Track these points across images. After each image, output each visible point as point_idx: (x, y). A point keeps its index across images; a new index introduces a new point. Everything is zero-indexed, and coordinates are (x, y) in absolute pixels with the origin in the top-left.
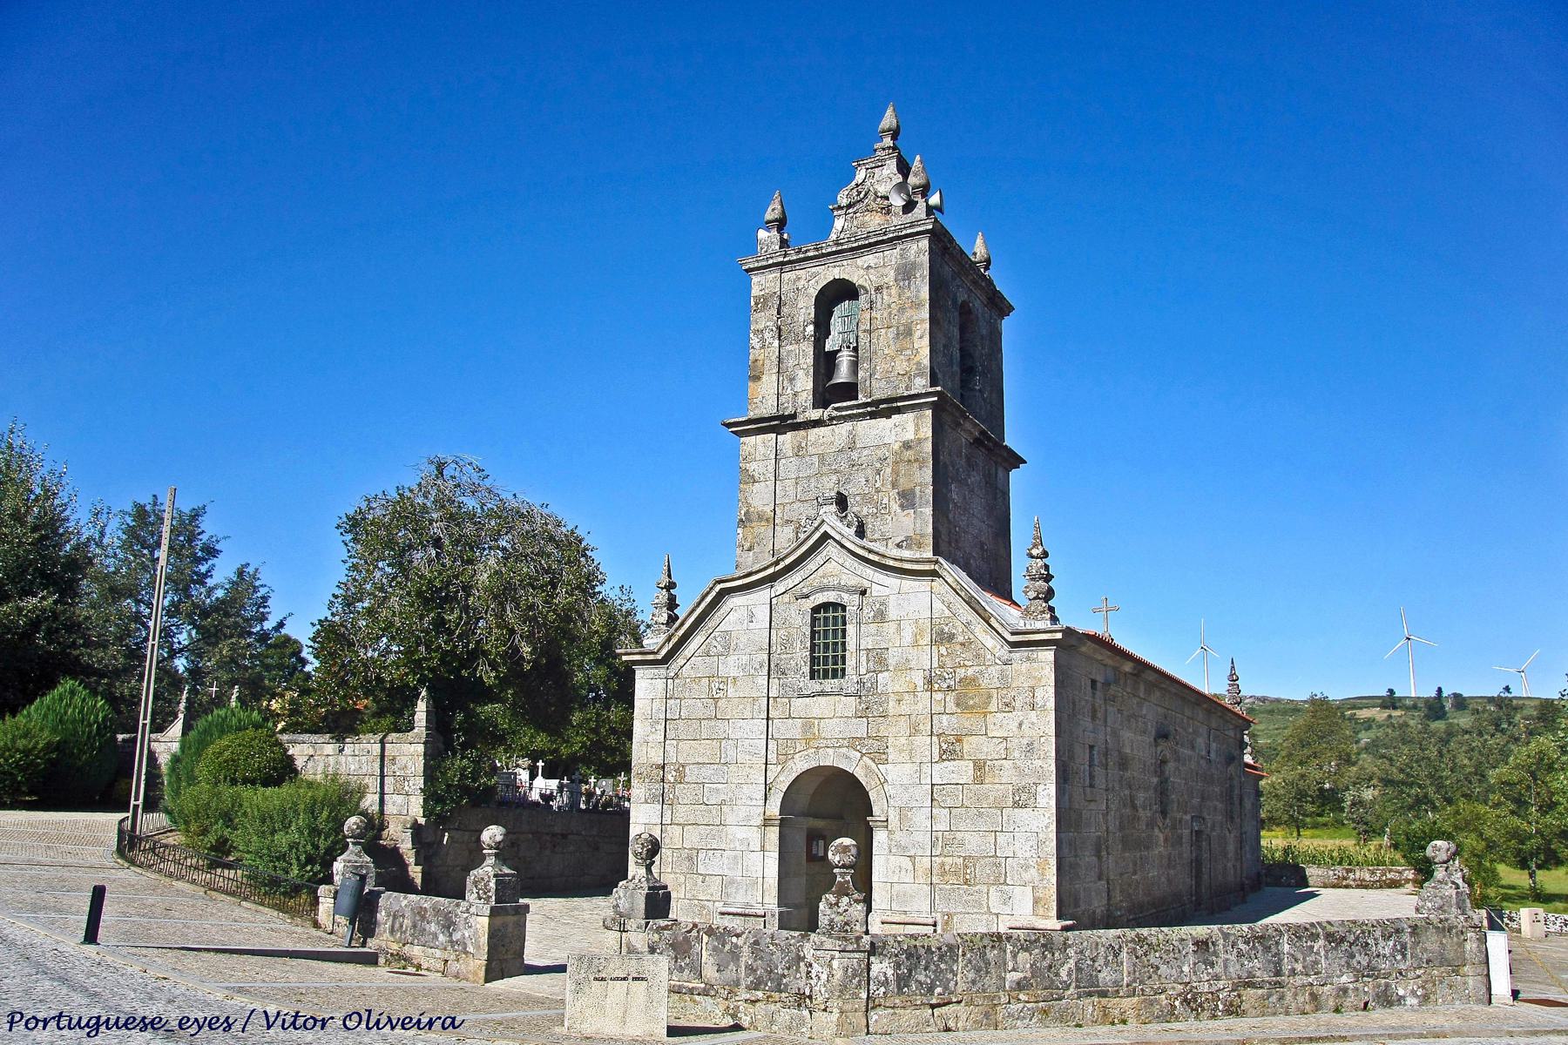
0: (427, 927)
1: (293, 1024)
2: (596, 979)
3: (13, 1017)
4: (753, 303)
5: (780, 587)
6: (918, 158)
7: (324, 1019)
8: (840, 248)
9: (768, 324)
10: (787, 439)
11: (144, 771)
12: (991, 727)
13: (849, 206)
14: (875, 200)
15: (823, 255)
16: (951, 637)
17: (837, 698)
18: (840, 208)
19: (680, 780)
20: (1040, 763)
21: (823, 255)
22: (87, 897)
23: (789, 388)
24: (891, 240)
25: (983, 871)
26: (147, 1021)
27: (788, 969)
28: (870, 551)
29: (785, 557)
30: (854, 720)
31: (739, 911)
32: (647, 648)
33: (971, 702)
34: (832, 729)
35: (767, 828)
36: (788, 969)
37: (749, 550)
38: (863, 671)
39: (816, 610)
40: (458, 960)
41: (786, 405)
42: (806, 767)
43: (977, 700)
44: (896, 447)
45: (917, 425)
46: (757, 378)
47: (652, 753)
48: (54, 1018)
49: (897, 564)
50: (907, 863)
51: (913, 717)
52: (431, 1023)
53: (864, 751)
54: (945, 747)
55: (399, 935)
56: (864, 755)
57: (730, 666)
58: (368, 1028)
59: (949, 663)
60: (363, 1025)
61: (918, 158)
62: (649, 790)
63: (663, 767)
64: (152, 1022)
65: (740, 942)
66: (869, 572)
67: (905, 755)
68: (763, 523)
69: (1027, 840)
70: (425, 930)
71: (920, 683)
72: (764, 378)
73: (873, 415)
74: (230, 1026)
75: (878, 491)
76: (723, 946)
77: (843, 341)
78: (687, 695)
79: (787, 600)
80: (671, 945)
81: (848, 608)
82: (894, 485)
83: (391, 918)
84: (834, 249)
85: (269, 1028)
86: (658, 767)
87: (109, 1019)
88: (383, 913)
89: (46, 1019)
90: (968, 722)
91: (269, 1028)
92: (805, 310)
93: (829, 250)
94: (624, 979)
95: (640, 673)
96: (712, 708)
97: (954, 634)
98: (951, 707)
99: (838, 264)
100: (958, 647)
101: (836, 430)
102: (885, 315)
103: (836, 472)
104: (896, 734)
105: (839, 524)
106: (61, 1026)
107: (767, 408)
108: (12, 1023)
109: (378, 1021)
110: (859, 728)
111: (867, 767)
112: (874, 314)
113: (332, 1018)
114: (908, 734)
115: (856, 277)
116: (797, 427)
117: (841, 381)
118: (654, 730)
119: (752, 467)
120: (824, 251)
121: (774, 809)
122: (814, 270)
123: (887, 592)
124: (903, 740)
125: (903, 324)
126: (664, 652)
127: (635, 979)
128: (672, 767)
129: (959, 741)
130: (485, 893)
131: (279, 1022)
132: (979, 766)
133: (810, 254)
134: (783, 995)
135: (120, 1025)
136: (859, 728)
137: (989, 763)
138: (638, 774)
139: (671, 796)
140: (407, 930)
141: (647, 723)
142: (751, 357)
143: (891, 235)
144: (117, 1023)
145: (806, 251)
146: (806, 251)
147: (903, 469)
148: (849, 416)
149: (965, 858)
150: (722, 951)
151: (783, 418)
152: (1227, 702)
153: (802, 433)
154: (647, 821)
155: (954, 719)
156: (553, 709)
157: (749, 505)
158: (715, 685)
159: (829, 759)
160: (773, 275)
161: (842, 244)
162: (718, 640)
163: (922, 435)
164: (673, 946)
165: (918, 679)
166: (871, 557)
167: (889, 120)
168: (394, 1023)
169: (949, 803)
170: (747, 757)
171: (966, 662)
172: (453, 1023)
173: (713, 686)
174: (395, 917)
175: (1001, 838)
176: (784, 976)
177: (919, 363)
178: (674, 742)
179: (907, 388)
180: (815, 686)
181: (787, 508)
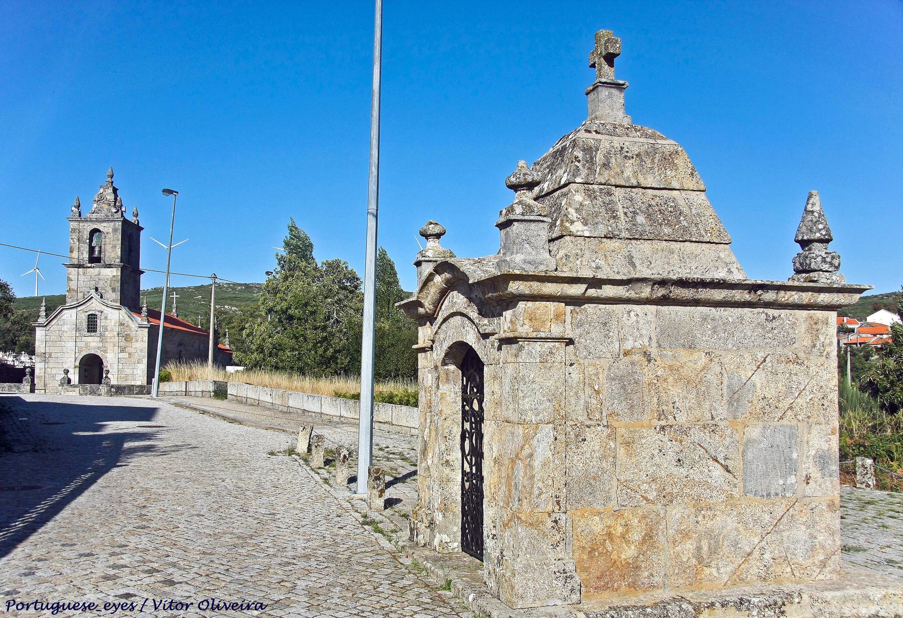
3: (9, 603)
5: (79, 309)
13: (99, 201)
26: (86, 605)
39: (89, 315)
48: (33, 603)
57: (65, 328)
64: (89, 606)
67: (112, 352)
72: (74, 252)
73: (105, 267)
92: (86, 235)
103: (95, 281)
104: (110, 347)
108: (9, 606)
121: (77, 364)
122: (89, 224)
123: (108, 312)
131: (162, 605)
132: (130, 354)
144: (69, 606)
159: (93, 352)
165: (116, 334)
169: (122, 362)
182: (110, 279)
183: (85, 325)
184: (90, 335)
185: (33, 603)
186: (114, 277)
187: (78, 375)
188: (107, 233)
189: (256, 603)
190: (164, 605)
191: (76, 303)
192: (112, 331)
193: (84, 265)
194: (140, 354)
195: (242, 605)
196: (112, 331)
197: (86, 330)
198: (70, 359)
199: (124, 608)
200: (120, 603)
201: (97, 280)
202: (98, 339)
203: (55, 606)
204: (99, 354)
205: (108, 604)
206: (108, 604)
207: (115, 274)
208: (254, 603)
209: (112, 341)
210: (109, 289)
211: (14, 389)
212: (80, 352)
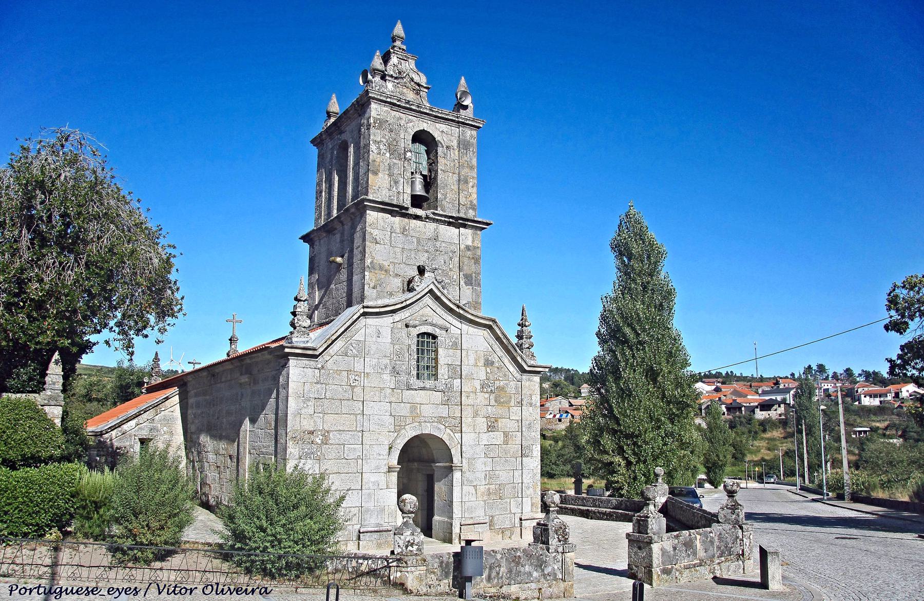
1: (174, 591)
3: (12, 588)
5: (397, 317)
7: (191, 589)
8: (431, 113)
9: (383, 139)
12: (511, 414)
16: (493, 363)
17: (431, 392)
19: (325, 442)
23: (395, 188)
24: (458, 122)
25: (508, 490)
26: (90, 590)
31: (376, 529)
32: (295, 345)
33: (502, 400)
34: (427, 411)
35: (390, 473)
42: (414, 434)
45: (473, 238)
47: (305, 423)
48: (35, 588)
49: (472, 318)
50: (472, 490)
51: (475, 407)
52: (253, 591)
53: (447, 425)
55: (496, 580)
56: (446, 427)
58: (217, 594)
60: (214, 592)
62: (302, 449)
64: (92, 591)
66: (450, 318)
71: (478, 387)
72: (380, 175)
73: (450, 224)
74: (137, 592)
75: (451, 270)
78: (331, 382)
80: (684, 544)
84: (428, 112)
85: (160, 593)
87: (67, 588)
89: (31, 589)
90: (500, 411)
91: (160, 593)
93: (425, 111)
95: (292, 362)
96: (350, 392)
98: (493, 402)
99: (425, 121)
101: (427, 225)
102: (452, 165)
106: (40, 593)
108: (11, 591)
109: (223, 589)
110: (443, 411)
113: (196, 588)
114: (472, 416)
115: (437, 136)
118: (305, 405)
122: (410, 117)
124: (470, 420)
128: (319, 433)
129: (496, 421)
131: (166, 590)
132: (506, 434)
133: (413, 107)
135: (74, 592)
136: (443, 411)
137: (510, 433)
138: (292, 437)
139: (319, 453)
143: (461, 120)
144: (72, 591)
145: (412, 105)
146: (412, 105)
148: (441, 220)
149: (500, 485)
153: (406, 220)
159: (427, 429)
161: (433, 111)
162: (354, 345)
168: (232, 591)
170: (377, 427)
172: (266, 591)
173: (350, 377)
177: (471, 202)
178: (321, 415)
181: (397, 266)
184: (422, 385)
185: (35, 588)
186: (469, 250)
188: (447, 147)
189: (260, 588)
190: (168, 589)
195: (246, 590)
199: (128, 593)
200: (123, 588)
203: (57, 591)
205: (111, 589)
206: (111, 589)
208: (258, 588)
211: (527, 568)
212: (398, 429)
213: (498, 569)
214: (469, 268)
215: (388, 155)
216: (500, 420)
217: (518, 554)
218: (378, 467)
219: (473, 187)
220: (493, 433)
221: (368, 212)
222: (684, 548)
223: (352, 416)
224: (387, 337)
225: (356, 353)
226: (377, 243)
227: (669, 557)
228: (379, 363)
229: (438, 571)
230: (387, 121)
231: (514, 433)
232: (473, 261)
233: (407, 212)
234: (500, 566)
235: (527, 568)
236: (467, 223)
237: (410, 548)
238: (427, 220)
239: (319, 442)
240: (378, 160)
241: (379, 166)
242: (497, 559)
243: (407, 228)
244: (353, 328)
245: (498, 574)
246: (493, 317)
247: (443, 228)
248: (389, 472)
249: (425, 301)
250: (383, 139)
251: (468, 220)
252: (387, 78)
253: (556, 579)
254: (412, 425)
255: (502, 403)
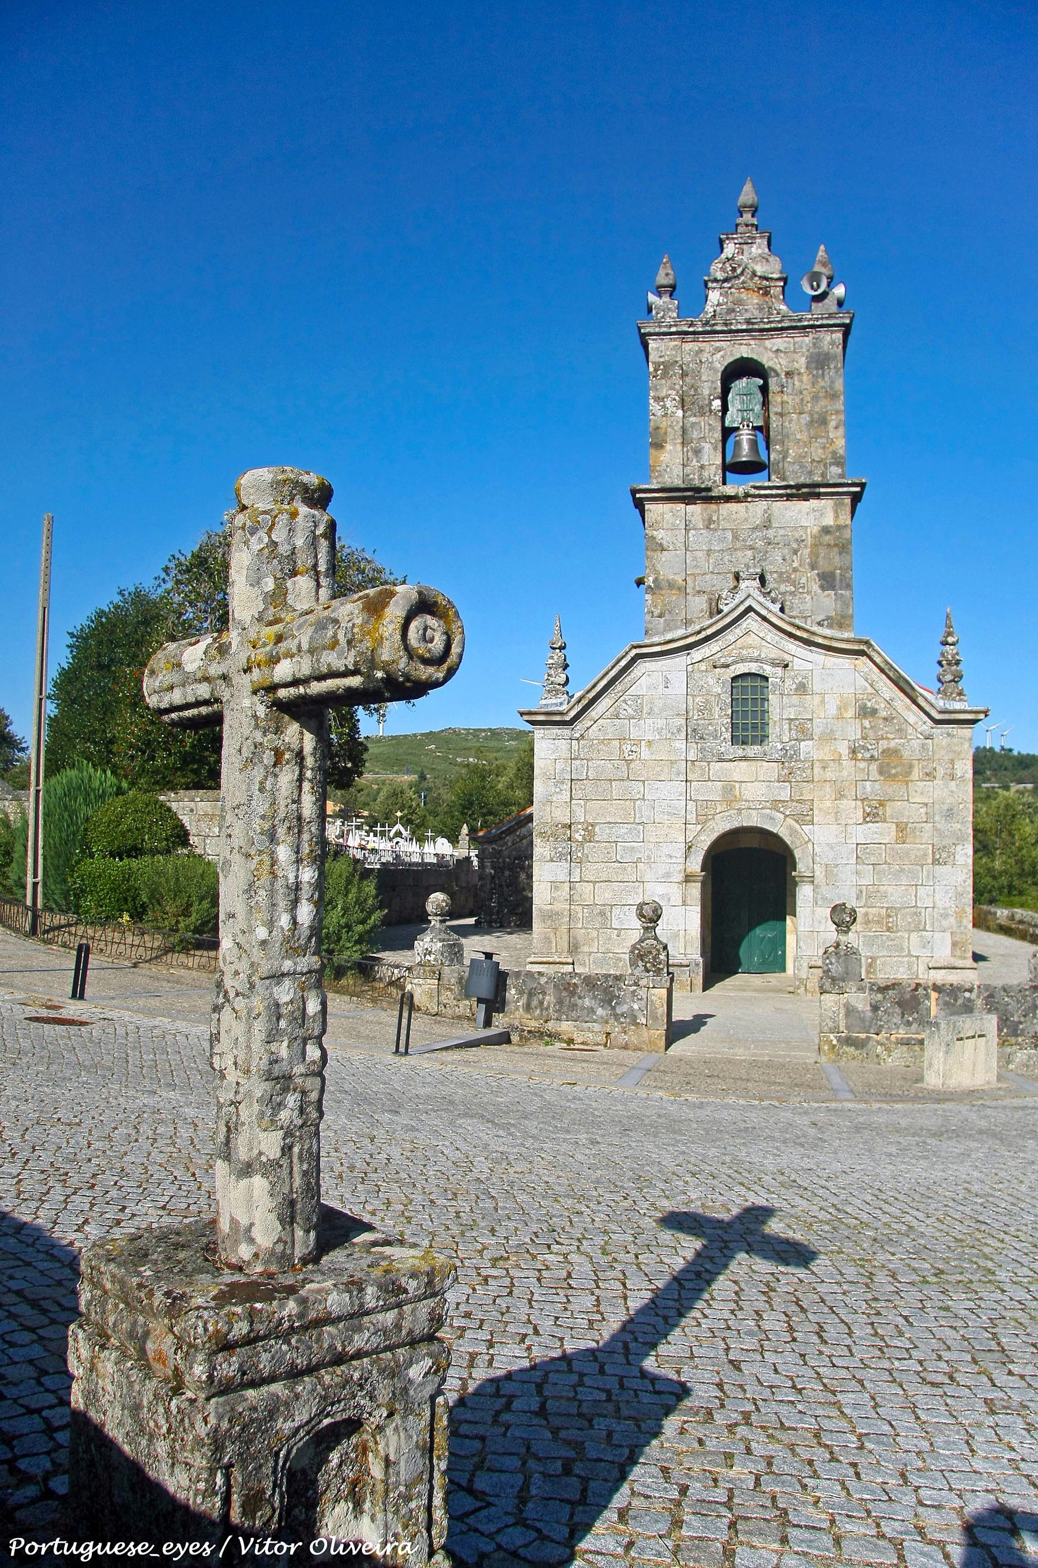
0: (580, 1002)
2: (958, 1040)
4: (651, 369)
5: (697, 654)
6: (822, 247)
8: (750, 327)
10: (696, 510)
11: (41, 844)
12: (912, 793)
13: (726, 280)
14: (752, 279)
15: (731, 331)
16: (874, 712)
17: (759, 763)
18: (716, 280)
20: (959, 826)
21: (731, 331)
22: (89, 991)
24: (805, 327)
27: (1025, 1016)
28: (799, 628)
29: (708, 627)
30: (777, 784)
33: (893, 771)
36: (1025, 1016)
37: (660, 616)
38: (786, 739)
39: (734, 679)
40: (625, 1032)
41: (691, 476)
43: (899, 769)
44: (815, 530)
45: (836, 512)
46: (659, 446)
53: (788, 813)
54: (868, 810)
55: (538, 1012)
57: (646, 729)
59: (871, 733)
61: (822, 247)
63: (570, 826)
65: (974, 996)
66: (792, 647)
67: (831, 818)
68: (674, 592)
69: (947, 892)
70: (576, 1005)
72: (669, 447)
73: (789, 497)
76: (956, 1000)
77: (743, 420)
78: (594, 756)
79: (703, 668)
80: (897, 1003)
81: (770, 680)
82: (813, 567)
83: (525, 996)
84: (744, 327)
86: (564, 826)
88: (513, 991)
90: (892, 788)
92: (710, 383)
93: (739, 327)
94: (973, 1037)
96: (624, 769)
97: (876, 710)
98: (874, 774)
99: (745, 342)
100: (881, 721)
102: (797, 400)
103: (751, 548)
104: (824, 802)
105: (761, 599)
107: (674, 478)
111: (791, 828)
112: (785, 398)
114: (833, 798)
115: (767, 360)
116: (709, 500)
117: (744, 459)
118: (558, 790)
119: (659, 535)
120: (733, 327)
121: (695, 865)
122: (718, 344)
123: (810, 666)
124: (828, 804)
125: (817, 413)
126: (573, 713)
127: (980, 1036)
130: (654, 966)
132: (901, 828)
133: (718, 328)
134: (1020, 1039)
137: (910, 825)
140: (549, 1006)
141: (551, 783)
142: (652, 424)
143: (806, 323)
145: (714, 325)
146: (714, 325)
147: (822, 552)
149: (887, 908)
150: (953, 1005)
151: (698, 490)
152: (287, 718)
153: (714, 507)
154: (553, 879)
155: (877, 785)
156: (349, 765)
157: (657, 572)
158: (627, 748)
159: (753, 820)
160: (674, 343)
161: (753, 324)
163: (841, 522)
164: (900, 1004)
165: (844, 749)
166: (799, 633)
167: (747, 194)
169: (873, 860)
171: (889, 736)
174: (531, 995)
175: (921, 891)
176: (1021, 1023)
177: (834, 453)
179: (823, 475)
180: (739, 751)
182: (809, 541)
183: (721, 719)
184: (740, 753)
187: (698, 909)
191: (680, 632)
192: (829, 737)
193: (709, 489)
194: (942, 825)
196: (829, 737)
197: (728, 736)
198: (666, 849)
201: (760, 543)
202: (772, 769)
204: (780, 826)
207: (829, 520)
209: (829, 775)
210: (810, 579)
211: (587, 1002)
213: (541, 996)
214: (835, 561)
215: (680, 413)
216: (888, 803)
217: (574, 981)
218: (668, 875)
219: (836, 428)
220: (877, 825)
221: (647, 507)
222: (898, 1010)
223: (628, 802)
224: (679, 687)
225: (632, 713)
226: (663, 550)
227: (863, 1020)
228: (667, 724)
229: (456, 989)
230: (677, 362)
231: (918, 826)
232: (836, 549)
233: (710, 494)
234: (544, 993)
235: (587, 1002)
236: (817, 490)
237: (428, 957)
238: (749, 499)
239: (580, 839)
240: (663, 425)
241: (666, 433)
242: (539, 983)
243: (715, 518)
244: (627, 679)
245: (541, 1003)
246: (865, 638)
247: (778, 506)
248: (686, 881)
249: (744, 625)
250: (670, 392)
251: (819, 486)
252: (710, 285)
253: (635, 1023)
254: (727, 814)
255: (895, 775)
